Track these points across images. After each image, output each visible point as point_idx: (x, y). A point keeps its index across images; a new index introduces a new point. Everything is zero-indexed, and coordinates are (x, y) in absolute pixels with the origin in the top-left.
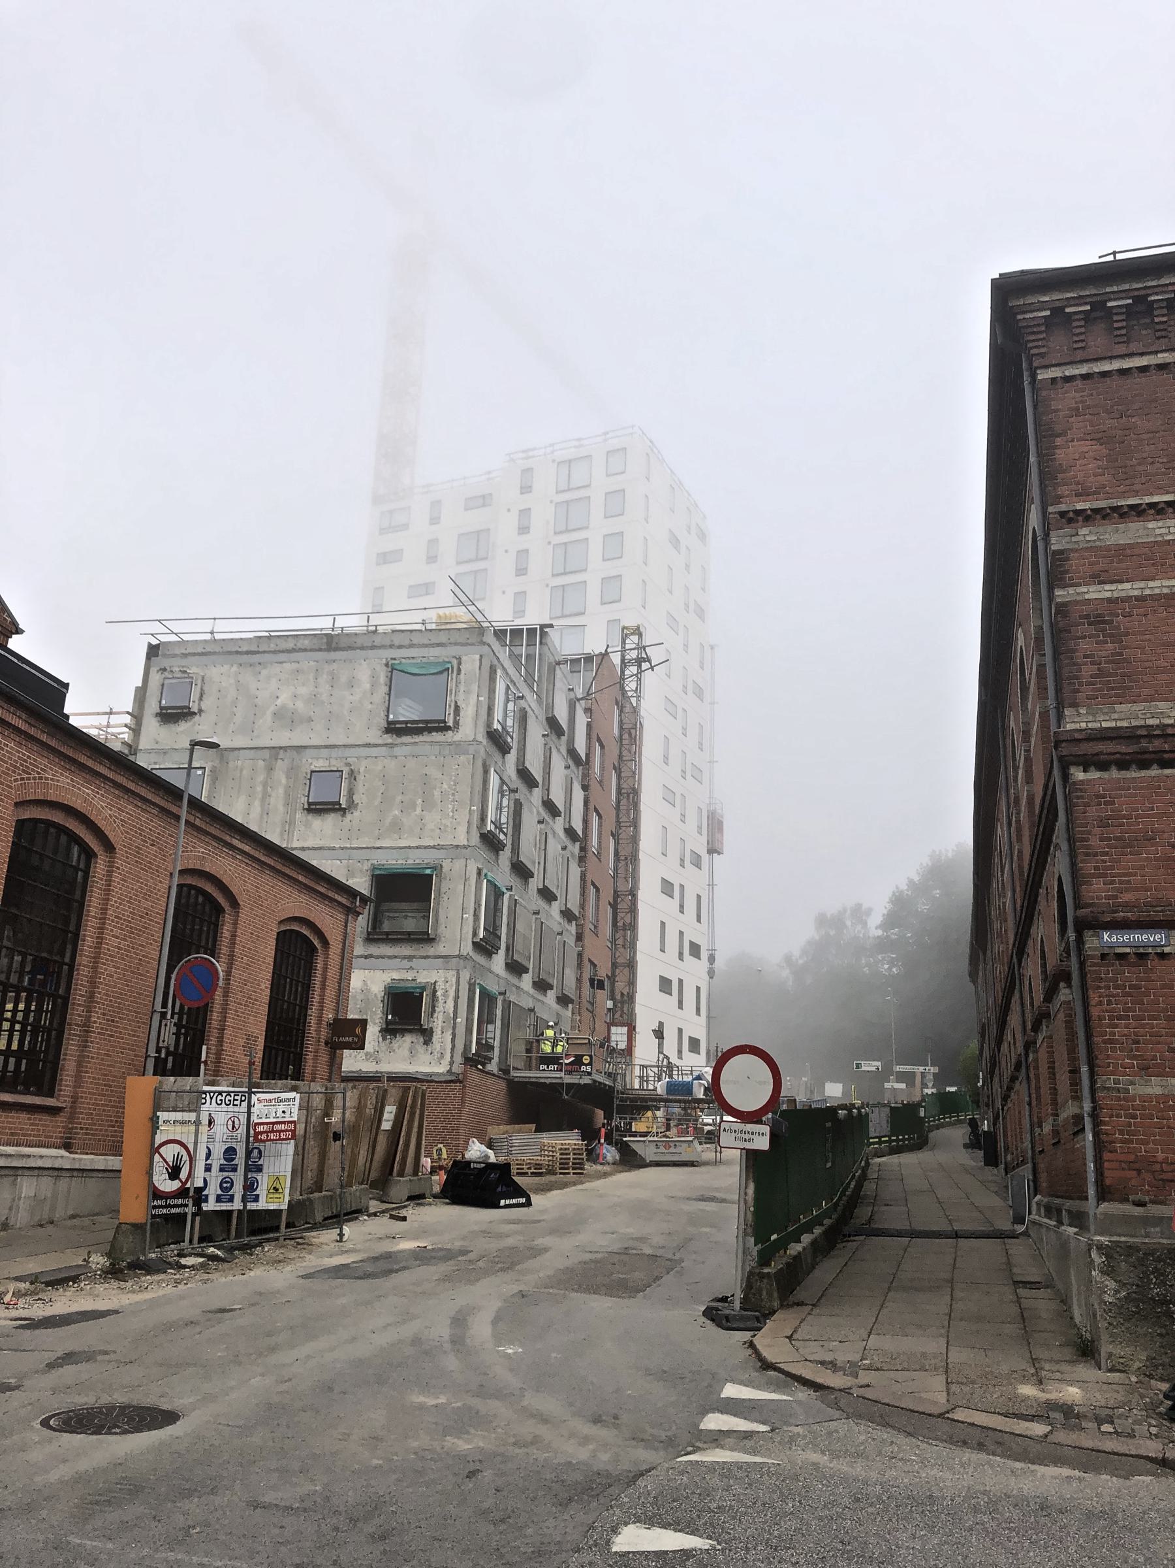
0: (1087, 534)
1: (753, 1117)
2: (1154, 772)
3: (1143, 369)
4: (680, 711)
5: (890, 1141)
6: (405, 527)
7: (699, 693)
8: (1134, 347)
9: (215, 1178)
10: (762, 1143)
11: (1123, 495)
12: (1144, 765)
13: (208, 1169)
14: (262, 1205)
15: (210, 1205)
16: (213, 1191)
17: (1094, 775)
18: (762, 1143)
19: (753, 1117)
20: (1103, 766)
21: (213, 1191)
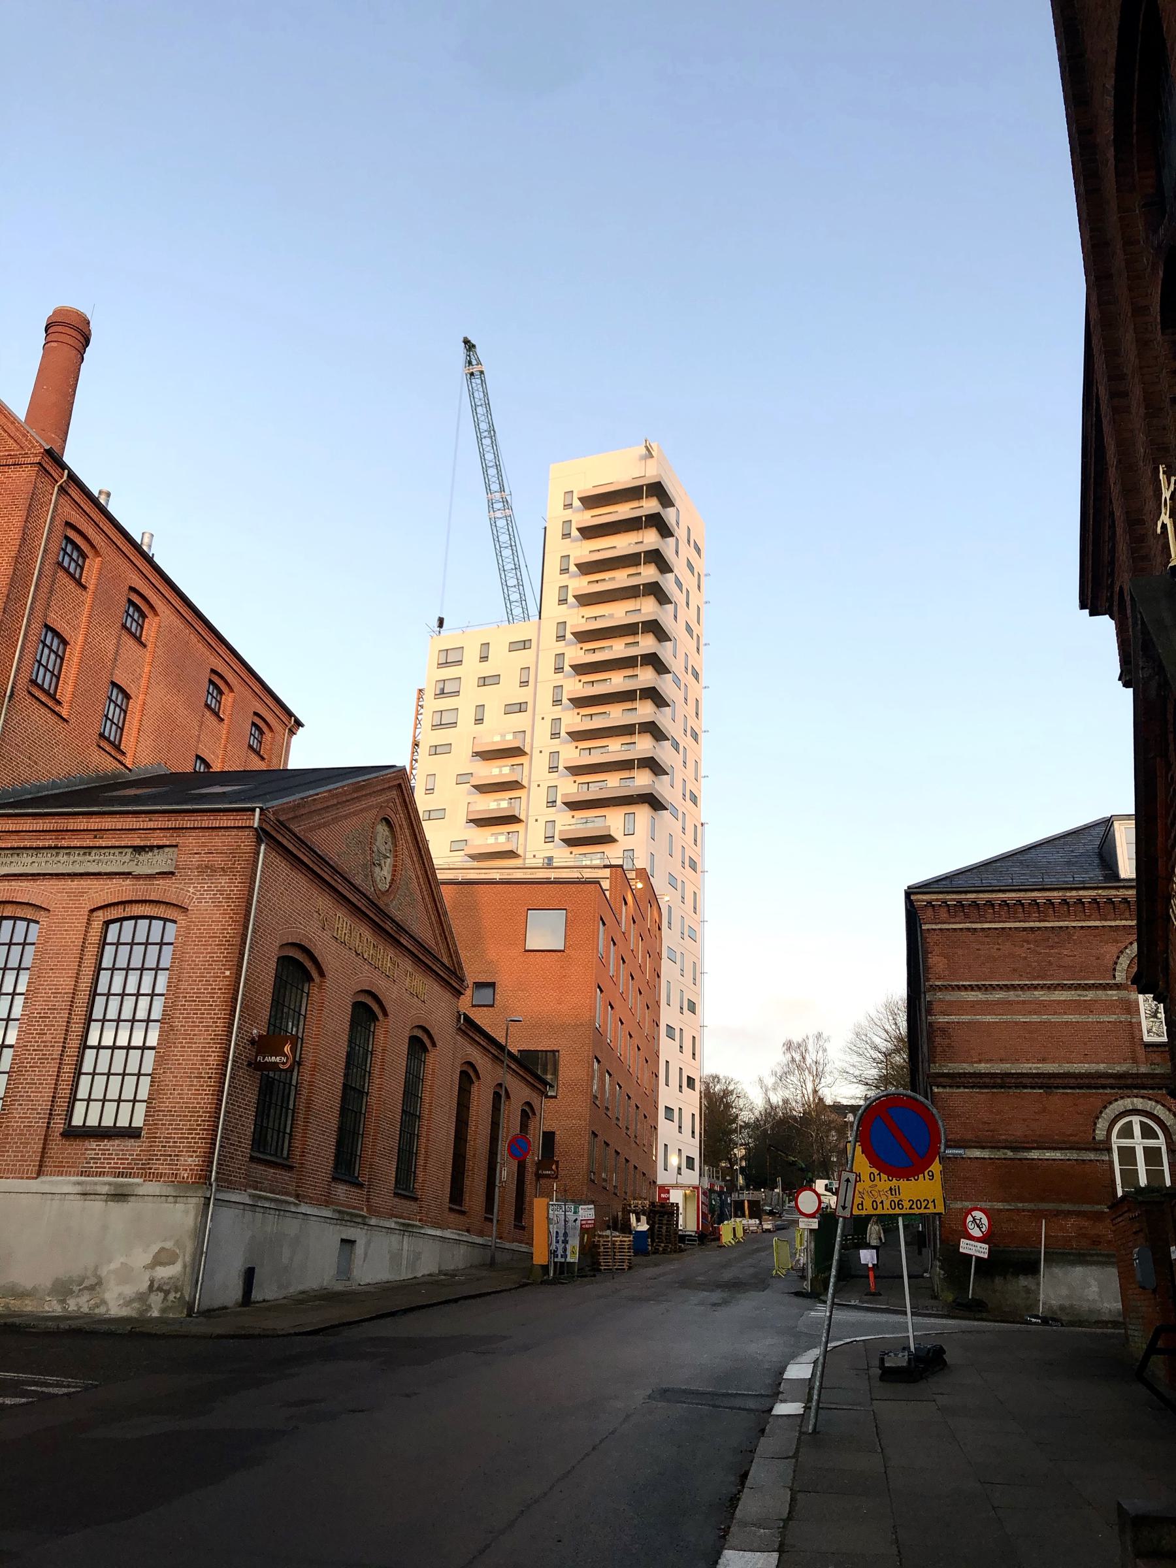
0: (940, 995)
1: (812, 1216)
2: (961, 1090)
3: (961, 929)
4: (679, 883)
5: (853, 1239)
6: (454, 724)
7: (693, 865)
8: (958, 919)
9: (561, 1246)
10: (815, 1226)
11: (953, 980)
12: (958, 1087)
13: (557, 1242)
14: (569, 1260)
15: (560, 1259)
16: (560, 1252)
17: (941, 1090)
18: (815, 1226)
19: (812, 1216)
20: (944, 1087)
21: (560, 1252)
